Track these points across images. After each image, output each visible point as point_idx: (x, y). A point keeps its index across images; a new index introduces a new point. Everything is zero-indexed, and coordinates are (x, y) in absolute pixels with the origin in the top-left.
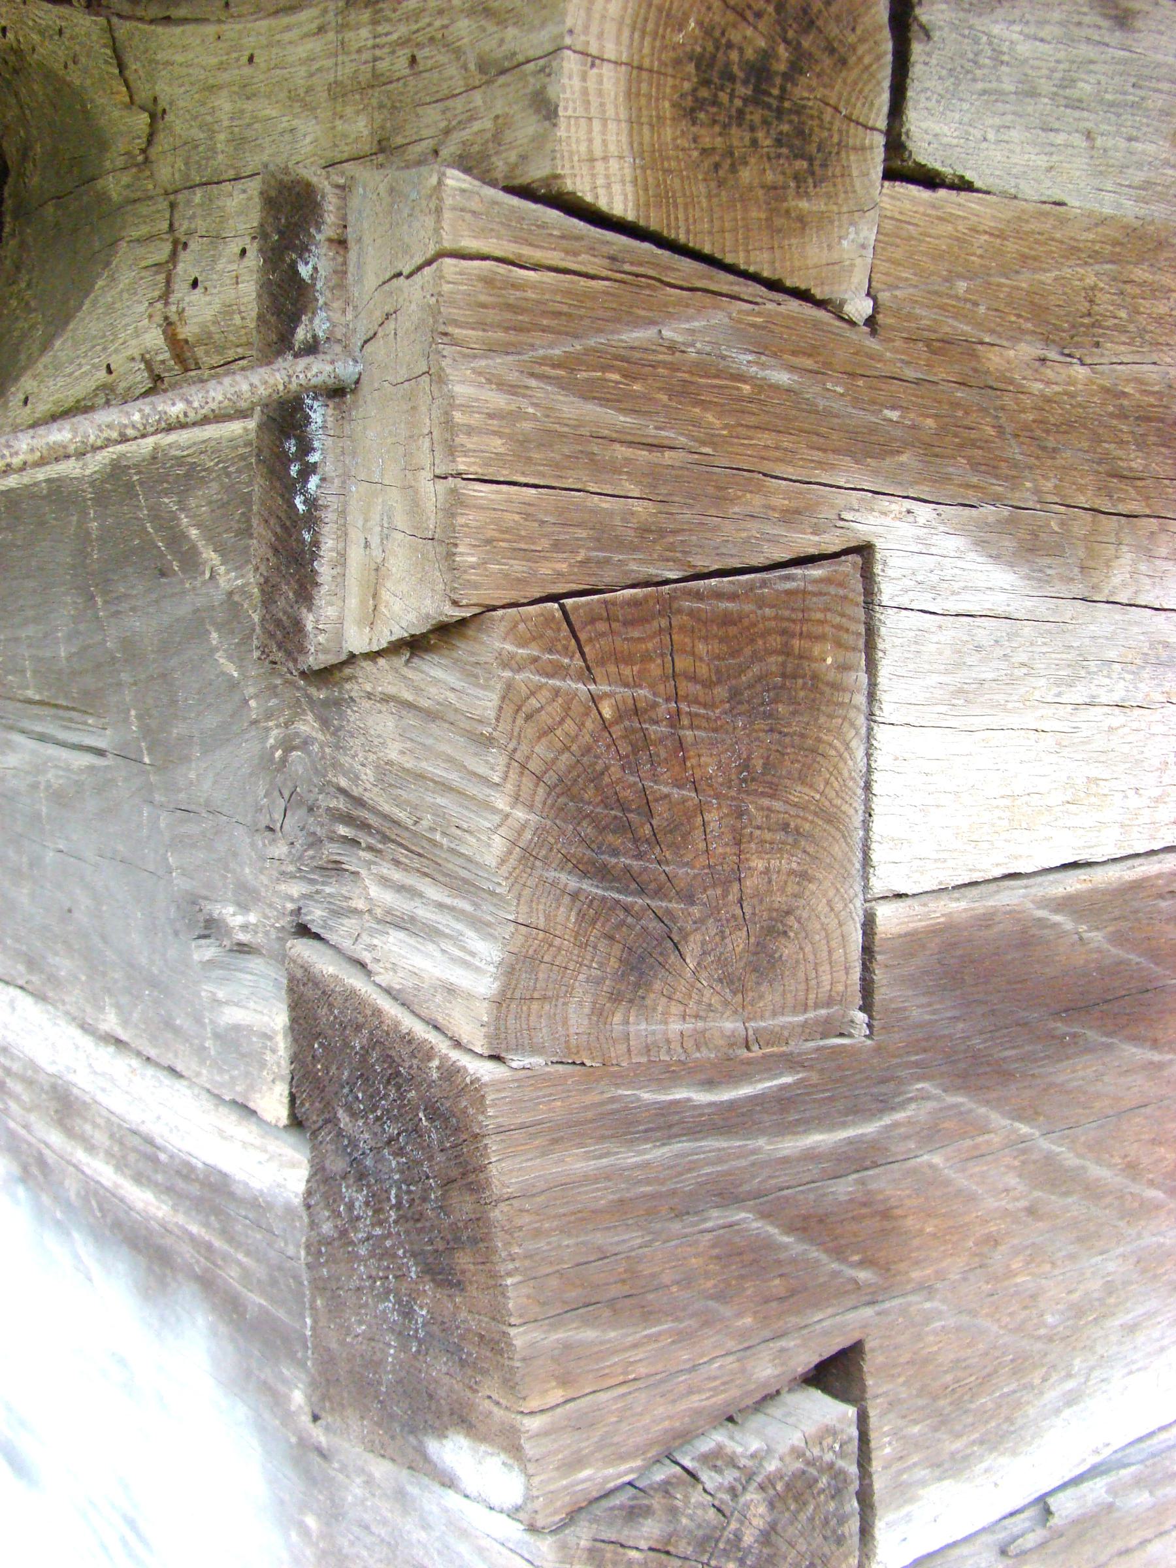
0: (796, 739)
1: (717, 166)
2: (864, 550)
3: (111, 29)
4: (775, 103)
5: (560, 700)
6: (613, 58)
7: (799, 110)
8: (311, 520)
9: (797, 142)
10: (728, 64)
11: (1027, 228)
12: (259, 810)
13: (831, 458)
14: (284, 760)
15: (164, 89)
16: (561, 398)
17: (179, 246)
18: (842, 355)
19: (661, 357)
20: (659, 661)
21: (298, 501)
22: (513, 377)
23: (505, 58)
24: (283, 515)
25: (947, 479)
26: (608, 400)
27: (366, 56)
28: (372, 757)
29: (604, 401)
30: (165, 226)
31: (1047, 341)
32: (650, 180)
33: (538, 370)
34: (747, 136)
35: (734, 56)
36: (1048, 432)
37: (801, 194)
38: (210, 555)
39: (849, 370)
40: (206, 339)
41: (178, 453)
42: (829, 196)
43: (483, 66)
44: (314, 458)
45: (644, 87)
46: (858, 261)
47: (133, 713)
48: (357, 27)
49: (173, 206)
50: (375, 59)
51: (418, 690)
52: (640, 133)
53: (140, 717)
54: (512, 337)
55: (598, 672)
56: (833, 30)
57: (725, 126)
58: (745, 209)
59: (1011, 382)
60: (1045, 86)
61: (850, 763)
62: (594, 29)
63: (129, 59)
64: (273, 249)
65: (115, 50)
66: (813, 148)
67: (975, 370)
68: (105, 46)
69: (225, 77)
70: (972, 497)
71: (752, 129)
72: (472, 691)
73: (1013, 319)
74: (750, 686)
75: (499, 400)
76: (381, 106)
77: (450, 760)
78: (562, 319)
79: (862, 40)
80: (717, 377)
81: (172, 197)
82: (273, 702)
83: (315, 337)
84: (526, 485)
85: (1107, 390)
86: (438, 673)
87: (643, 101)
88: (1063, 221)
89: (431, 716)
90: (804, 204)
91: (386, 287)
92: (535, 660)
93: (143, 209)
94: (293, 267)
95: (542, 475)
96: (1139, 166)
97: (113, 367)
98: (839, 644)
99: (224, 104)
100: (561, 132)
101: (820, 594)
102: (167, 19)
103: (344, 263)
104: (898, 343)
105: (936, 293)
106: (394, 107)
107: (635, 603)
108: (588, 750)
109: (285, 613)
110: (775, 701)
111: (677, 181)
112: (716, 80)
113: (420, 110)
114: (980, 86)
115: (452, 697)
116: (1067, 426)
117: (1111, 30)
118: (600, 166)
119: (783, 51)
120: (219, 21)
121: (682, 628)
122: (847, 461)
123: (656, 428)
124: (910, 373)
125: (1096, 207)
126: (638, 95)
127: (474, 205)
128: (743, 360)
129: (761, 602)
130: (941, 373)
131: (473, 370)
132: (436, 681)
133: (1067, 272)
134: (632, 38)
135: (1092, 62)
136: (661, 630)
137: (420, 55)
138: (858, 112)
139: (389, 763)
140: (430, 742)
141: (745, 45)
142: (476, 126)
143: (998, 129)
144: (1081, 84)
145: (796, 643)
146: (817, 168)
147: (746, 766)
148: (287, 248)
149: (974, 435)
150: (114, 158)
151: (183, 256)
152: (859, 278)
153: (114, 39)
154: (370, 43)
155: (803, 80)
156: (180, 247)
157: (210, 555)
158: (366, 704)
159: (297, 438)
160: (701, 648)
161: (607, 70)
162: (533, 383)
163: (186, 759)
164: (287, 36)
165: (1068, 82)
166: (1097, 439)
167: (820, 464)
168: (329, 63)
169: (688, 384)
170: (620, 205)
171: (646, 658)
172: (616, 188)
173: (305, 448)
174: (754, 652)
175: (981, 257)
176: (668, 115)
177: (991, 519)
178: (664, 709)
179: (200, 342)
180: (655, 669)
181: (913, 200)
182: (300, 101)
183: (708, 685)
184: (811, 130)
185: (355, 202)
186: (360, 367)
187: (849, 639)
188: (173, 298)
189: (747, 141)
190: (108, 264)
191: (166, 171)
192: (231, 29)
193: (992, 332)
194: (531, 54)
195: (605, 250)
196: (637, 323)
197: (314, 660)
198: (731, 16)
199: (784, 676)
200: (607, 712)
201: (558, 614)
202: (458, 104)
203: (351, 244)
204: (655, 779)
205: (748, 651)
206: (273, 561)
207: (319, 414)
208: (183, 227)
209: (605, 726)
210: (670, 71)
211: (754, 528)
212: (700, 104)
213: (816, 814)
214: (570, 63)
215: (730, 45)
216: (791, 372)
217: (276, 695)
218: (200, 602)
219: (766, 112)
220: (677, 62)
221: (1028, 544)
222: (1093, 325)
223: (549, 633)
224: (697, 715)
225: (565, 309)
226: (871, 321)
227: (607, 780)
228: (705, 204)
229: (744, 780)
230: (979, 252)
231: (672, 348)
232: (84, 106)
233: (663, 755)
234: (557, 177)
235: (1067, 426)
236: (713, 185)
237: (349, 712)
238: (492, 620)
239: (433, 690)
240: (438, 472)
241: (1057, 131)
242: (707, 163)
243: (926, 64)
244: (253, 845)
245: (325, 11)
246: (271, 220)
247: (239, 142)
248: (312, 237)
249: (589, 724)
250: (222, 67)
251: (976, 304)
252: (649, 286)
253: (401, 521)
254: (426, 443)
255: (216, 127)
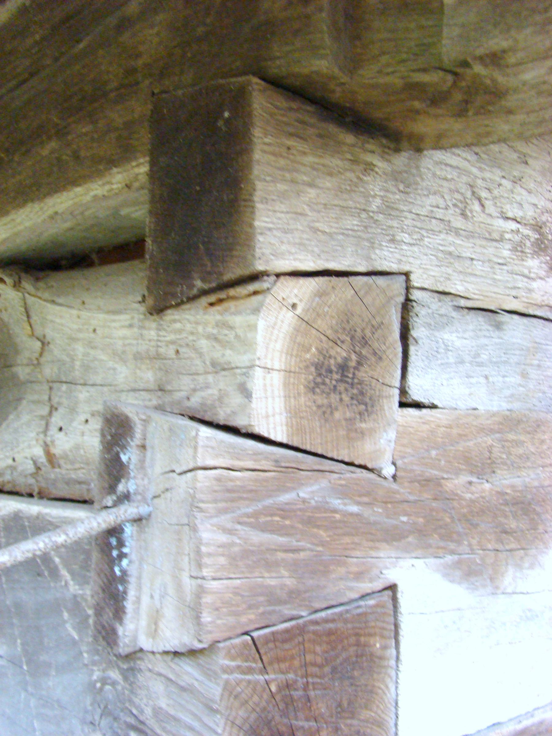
0: (363, 687)
1: (324, 413)
2: (392, 588)
3: (24, 299)
4: (350, 380)
5: (251, 686)
6: (278, 368)
7: (361, 383)
8: (124, 578)
9: (360, 397)
10: (329, 366)
11: (461, 422)
12: (86, 711)
13: (377, 544)
14: (101, 689)
15: (50, 333)
16: (251, 533)
17: (53, 409)
18: (381, 492)
19: (298, 506)
20: (298, 659)
21: (117, 570)
22: (229, 525)
23: (226, 363)
24: (108, 574)
25: (429, 546)
26: (273, 531)
27: (153, 343)
28: (151, 703)
29: (272, 532)
30: (46, 397)
31: (472, 473)
32: (294, 423)
33: (241, 520)
34: (338, 397)
35: (332, 361)
36: (473, 516)
37: (362, 420)
38: (64, 572)
39: (384, 500)
40: (65, 456)
41: (50, 519)
42: (374, 420)
43: (214, 364)
44: (125, 550)
45: (292, 380)
46: (388, 449)
47: (19, 641)
48: (150, 329)
49: (51, 388)
50: (158, 346)
51: (178, 675)
52: (290, 402)
53: (23, 644)
54: (229, 504)
55: (269, 668)
56: (376, 345)
57: (328, 394)
58: (337, 431)
59: (457, 495)
60: (467, 358)
61: (388, 695)
62: (269, 356)
63: (32, 314)
64: (108, 443)
65: (26, 309)
66: (367, 400)
67: (440, 491)
68: (21, 306)
69: (81, 336)
70: (441, 552)
71: (340, 393)
72: (207, 682)
73: (456, 464)
74: (341, 664)
75: (223, 538)
76: (160, 369)
77: (195, 715)
78: (252, 493)
79: (388, 348)
80: (325, 512)
81: (51, 384)
82: (96, 658)
83: (128, 491)
84: (236, 578)
85: (498, 492)
86: (189, 669)
87: (291, 387)
88: (477, 417)
89: (183, 689)
90: (363, 425)
91: (167, 475)
92: (239, 667)
93: (36, 387)
94: (118, 454)
95: (243, 572)
96: (508, 388)
97: (16, 459)
98: (382, 636)
99: (80, 349)
100: (254, 405)
101: (373, 613)
102: (53, 302)
103: (145, 457)
104: (406, 484)
105: (423, 458)
106: (167, 371)
107: (287, 631)
108: (264, 709)
109: (107, 622)
110: (353, 669)
111: (306, 422)
112: (324, 374)
113: (181, 376)
114: (439, 362)
115: (196, 684)
116: (482, 512)
117: (494, 331)
118: (271, 419)
119: (354, 357)
120: (80, 310)
121: (309, 641)
122: (384, 545)
123: (297, 541)
124: (412, 498)
125: (490, 408)
126: (289, 383)
127: (213, 444)
128: (336, 503)
129: (346, 621)
130: (426, 496)
131: (212, 525)
132: (188, 673)
133: (479, 440)
134: (286, 359)
135: (487, 345)
136: (299, 643)
137: (181, 350)
138: (387, 381)
139: (161, 708)
140: (183, 702)
141: (337, 356)
142: (210, 391)
143: (447, 380)
144: (483, 356)
145: (362, 639)
146: (369, 409)
147: (340, 705)
148: (115, 444)
149: (441, 523)
150: (22, 358)
151: (54, 413)
152: (388, 457)
153: (25, 303)
154: (155, 338)
155: (362, 369)
156: (53, 409)
157: (64, 572)
158: (148, 674)
159: (117, 537)
160: (318, 649)
161: (275, 374)
162: (239, 527)
163: (47, 675)
164: (113, 324)
165: (478, 355)
166: (495, 516)
167: (371, 548)
168: (134, 342)
169: (311, 518)
170: (279, 438)
171: (292, 658)
172: (279, 428)
173: (121, 544)
174: (343, 647)
175: (442, 438)
176: (302, 391)
177: (450, 563)
178: (301, 682)
179: (62, 458)
180: (296, 663)
181: (411, 416)
182: (120, 356)
183: (321, 666)
184: (366, 391)
185: (151, 428)
186: (151, 509)
187: (386, 633)
188: (50, 433)
189: (338, 400)
190: (16, 408)
191: (49, 371)
192: (85, 314)
193: (448, 472)
194: (239, 365)
195: (273, 457)
196: (287, 490)
197: (123, 650)
198: (331, 344)
199: (357, 656)
200: (273, 688)
201: (250, 642)
202: (201, 379)
203: (148, 447)
204: (296, 719)
205: (340, 647)
206: (101, 595)
207: (129, 530)
208: (55, 400)
209: (273, 696)
210: (304, 371)
211: (342, 585)
212: (317, 384)
213: (373, 724)
214: (258, 372)
215: (330, 357)
216: (358, 505)
217: (98, 654)
218: (58, 595)
219: (347, 385)
220: (307, 367)
221: (467, 572)
222: (492, 463)
223: (247, 652)
224: (317, 683)
225: (254, 488)
226: (394, 477)
227: (273, 723)
228: (318, 430)
229: (339, 713)
230: (440, 436)
231: (304, 501)
232: (8, 330)
233: (300, 705)
234: (250, 425)
235: (482, 512)
236: (323, 421)
237: (139, 676)
238: (218, 648)
239: (186, 677)
240: (192, 574)
241: (473, 377)
242: (320, 412)
243: (416, 355)
244: (83, 731)
245: (133, 318)
246: (107, 429)
247: (86, 368)
248: (128, 442)
249: (265, 696)
250: (80, 330)
251: (439, 460)
252: (293, 472)
253: (171, 591)
254: (186, 559)
255: (75, 358)
